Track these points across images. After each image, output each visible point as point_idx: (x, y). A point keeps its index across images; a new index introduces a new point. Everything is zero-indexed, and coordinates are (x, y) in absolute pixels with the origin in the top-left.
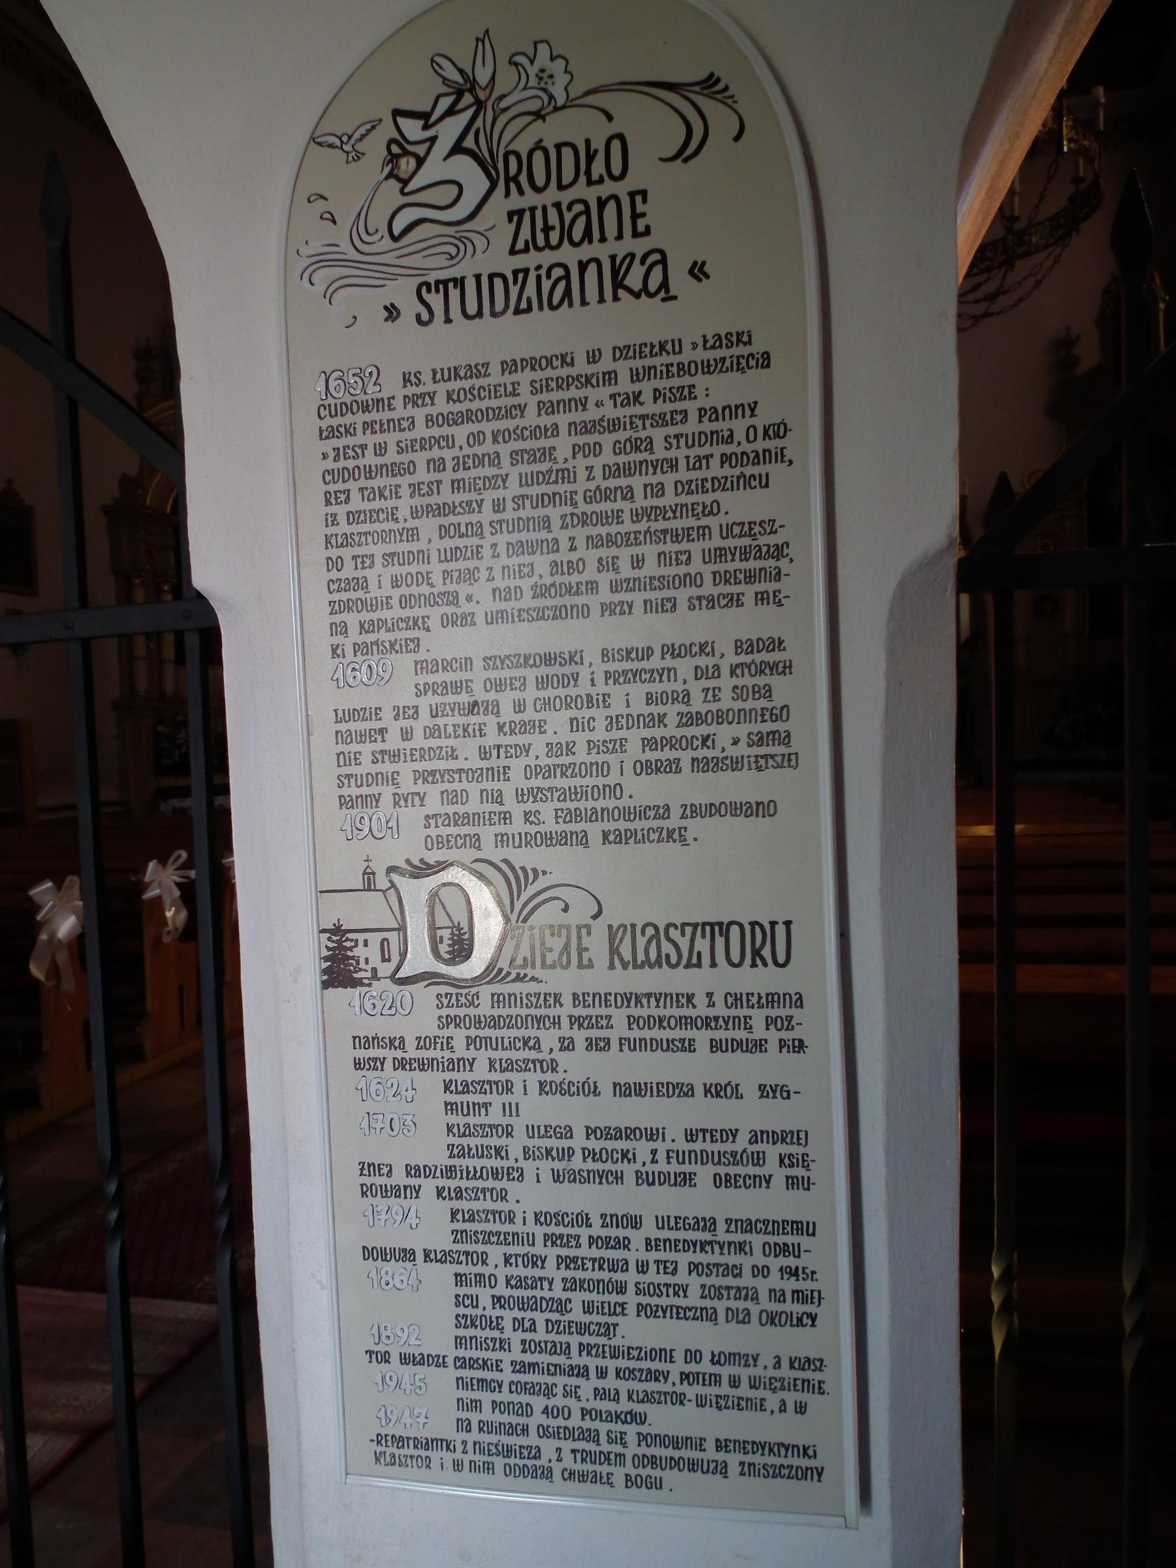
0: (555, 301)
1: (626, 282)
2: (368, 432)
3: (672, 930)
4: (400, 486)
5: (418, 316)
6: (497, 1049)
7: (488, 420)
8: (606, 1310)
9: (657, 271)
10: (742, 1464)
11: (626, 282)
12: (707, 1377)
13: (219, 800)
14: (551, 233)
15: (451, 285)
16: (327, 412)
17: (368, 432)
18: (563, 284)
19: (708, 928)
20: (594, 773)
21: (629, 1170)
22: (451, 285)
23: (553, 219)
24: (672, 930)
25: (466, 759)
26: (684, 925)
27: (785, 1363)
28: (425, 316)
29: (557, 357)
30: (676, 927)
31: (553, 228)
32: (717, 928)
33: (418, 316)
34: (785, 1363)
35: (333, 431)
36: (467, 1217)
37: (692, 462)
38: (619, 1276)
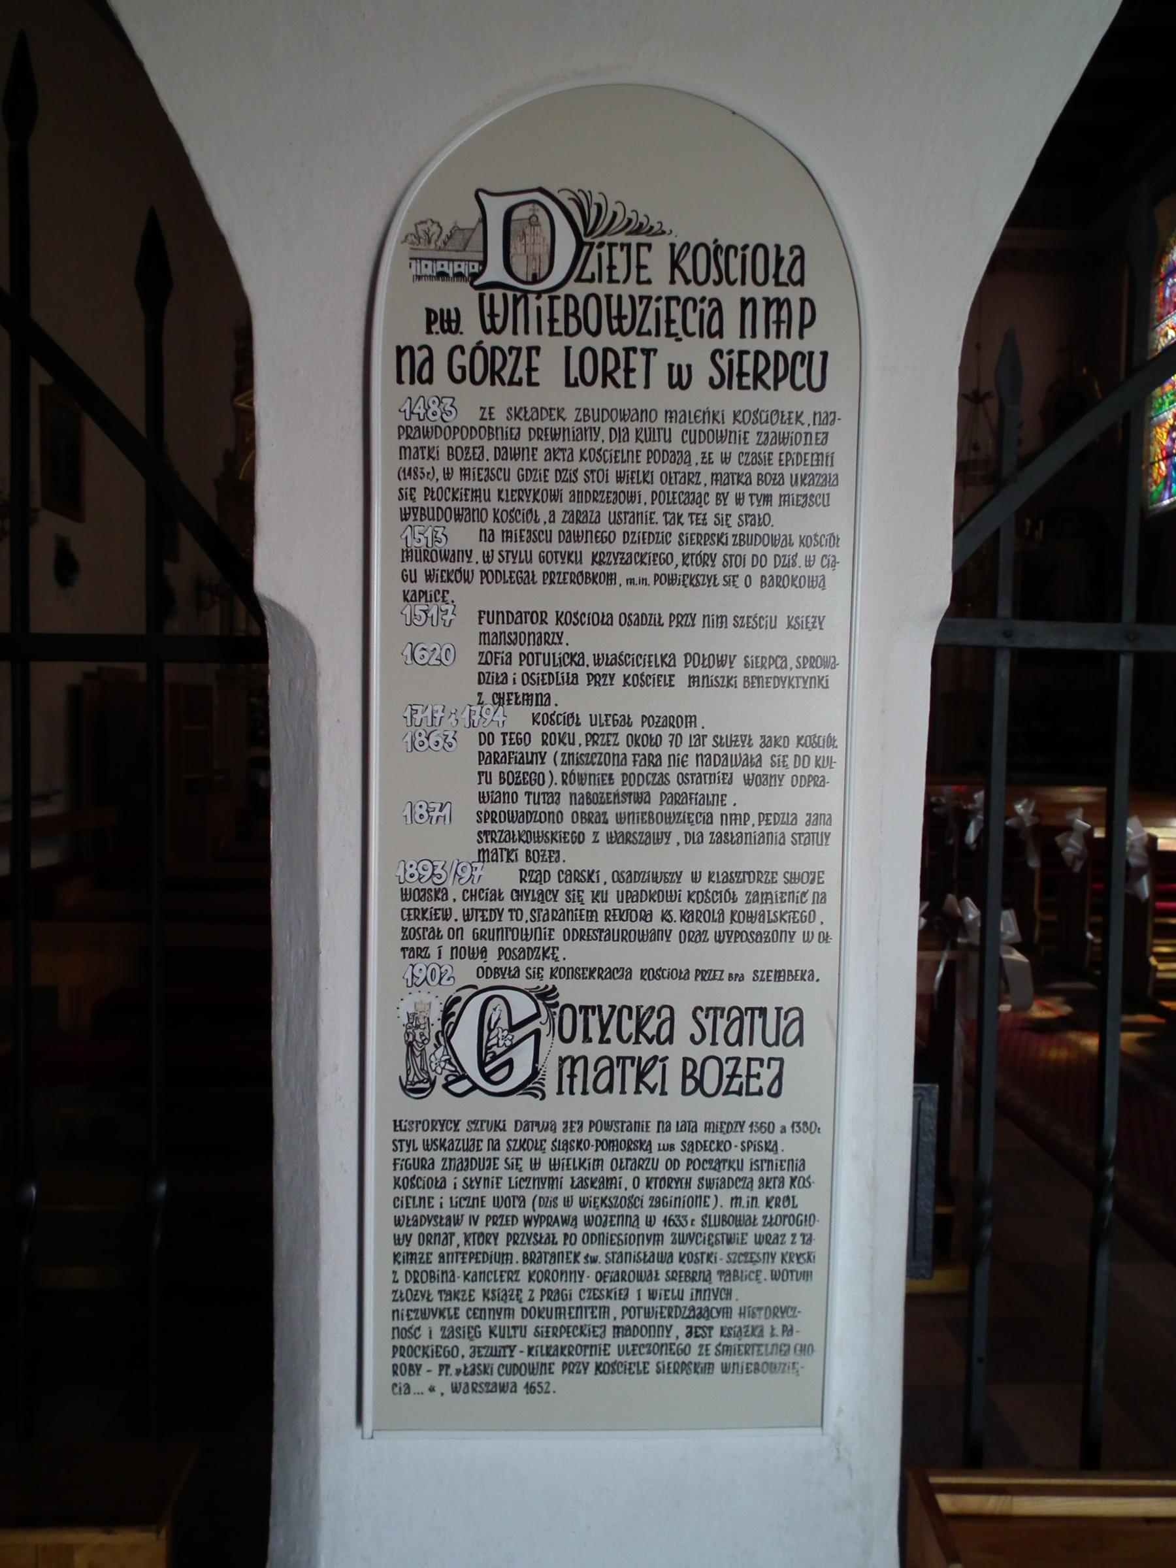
1: (644, 1030)
2: (473, 1261)
6: (777, 353)
8: (619, 458)
9: (667, 1026)
11: (644, 1030)
14: (496, 319)
15: (628, 1062)
17: (473, 1261)
18: (738, 1022)
19: (712, 1012)
21: (637, 729)
22: (628, 1062)
23: (627, 310)
26: (708, 1009)
27: (589, 837)
31: (626, 317)
34: (589, 837)
36: (721, 879)
38: (687, 927)
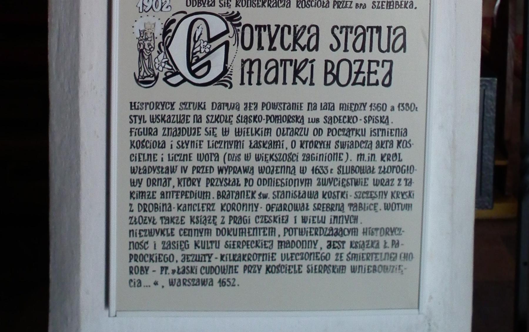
0: (396, 48)
3: (336, 29)
4: (201, 128)
5: (331, 46)
7: (281, 116)
10: (163, 243)
12: (208, 168)
13: (500, 210)
16: (205, 271)
20: (239, 147)
24: (336, 29)
25: (154, 271)
26: (342, 27)
28: (335, 46)
29: (148, 255)
30: (338, 28)
32: (349, 30)
33: (331, 46)
35: (170, 244)
37: (323, 105)
